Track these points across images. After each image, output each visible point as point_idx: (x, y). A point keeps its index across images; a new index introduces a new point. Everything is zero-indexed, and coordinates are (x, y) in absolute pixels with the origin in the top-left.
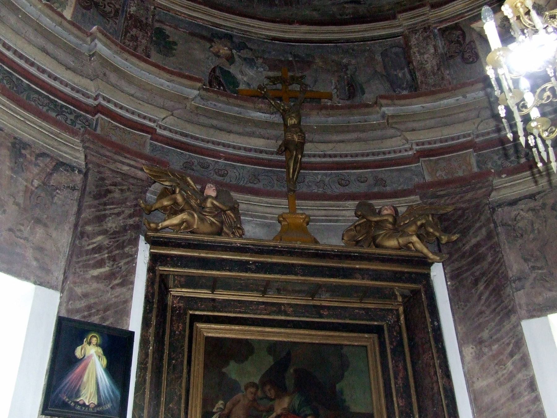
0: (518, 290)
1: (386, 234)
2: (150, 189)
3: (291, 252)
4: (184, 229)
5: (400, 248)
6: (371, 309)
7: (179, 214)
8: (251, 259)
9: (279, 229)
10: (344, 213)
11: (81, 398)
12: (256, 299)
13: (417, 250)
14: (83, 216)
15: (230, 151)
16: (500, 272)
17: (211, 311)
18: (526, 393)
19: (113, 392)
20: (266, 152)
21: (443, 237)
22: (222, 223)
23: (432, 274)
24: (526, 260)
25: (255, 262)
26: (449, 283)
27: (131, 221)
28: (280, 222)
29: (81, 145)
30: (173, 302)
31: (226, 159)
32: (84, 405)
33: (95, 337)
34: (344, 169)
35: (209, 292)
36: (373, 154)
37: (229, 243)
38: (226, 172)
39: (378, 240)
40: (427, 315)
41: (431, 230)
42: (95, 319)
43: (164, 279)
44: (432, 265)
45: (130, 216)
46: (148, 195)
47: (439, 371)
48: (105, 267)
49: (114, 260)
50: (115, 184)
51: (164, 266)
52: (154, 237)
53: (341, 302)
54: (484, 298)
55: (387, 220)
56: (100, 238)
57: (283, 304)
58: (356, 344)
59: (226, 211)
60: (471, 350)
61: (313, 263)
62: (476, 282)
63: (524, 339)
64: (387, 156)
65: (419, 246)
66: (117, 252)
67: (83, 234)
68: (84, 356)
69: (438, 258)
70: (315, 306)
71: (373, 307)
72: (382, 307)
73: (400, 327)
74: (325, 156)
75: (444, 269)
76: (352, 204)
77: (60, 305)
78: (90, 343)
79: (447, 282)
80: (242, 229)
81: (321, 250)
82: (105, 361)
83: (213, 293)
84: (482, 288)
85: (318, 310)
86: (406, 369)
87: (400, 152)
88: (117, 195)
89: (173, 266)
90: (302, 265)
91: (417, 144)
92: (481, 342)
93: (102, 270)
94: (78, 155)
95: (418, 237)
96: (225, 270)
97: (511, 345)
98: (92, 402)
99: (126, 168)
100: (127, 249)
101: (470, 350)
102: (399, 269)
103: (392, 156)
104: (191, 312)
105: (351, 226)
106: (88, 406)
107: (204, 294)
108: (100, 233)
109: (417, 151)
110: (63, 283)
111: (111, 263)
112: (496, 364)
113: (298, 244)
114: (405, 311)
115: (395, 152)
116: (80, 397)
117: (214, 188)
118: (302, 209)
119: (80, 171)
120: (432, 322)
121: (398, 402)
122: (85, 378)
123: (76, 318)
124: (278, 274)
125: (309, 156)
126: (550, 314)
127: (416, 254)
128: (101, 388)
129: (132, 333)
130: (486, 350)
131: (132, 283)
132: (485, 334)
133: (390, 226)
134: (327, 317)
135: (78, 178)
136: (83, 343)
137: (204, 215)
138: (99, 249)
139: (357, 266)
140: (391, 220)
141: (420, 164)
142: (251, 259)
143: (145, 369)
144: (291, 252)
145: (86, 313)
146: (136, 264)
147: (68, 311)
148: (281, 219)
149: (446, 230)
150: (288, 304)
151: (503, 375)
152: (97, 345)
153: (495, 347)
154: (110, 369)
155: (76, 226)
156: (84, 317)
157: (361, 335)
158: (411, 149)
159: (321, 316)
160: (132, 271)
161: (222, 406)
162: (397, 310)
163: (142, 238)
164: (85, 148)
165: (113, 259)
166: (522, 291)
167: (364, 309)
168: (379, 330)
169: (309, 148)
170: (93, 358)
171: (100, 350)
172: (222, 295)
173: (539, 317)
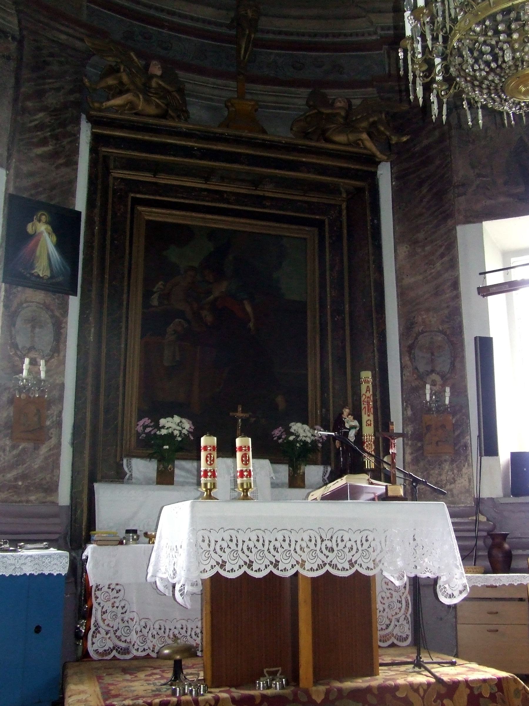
0: (459, 195)
1: (337, 128)
2: (89, 62)
3: (238, 141)
4: (129, 110)
5: (349, 144)
6: (314, 202)
7: (124, 95)
8: (196, 145)
9: (226, 113)
10: (296, 100)
11: (36, 271)
12: (199, 186)
13: (365, 148)
14: (23, 90)
15: (176, 19)
16: (446, 176)
17: (153, 195)
18: (448, 291)
19: (64, 267)
20: (216, 24)
21: (393, 137)
22: (167, 105)
23: (379, 172)
24: (473, 167)
25: (199, 149)
26: (393, 183)
27: (72, 98)
28: (227, 106)
29: (14, 7)
30: (114, 184)
31: (170, 29)
32: (38, 276)
33: (43, 214)
34: (300, 49)
35: (151, 176)
36: (334, 35)
37: (175, 127)
38: (170, 45)
39: (328, 134)
40: (368, 213)
41: (382, 129)
42: (42, 198)
43: (106, 158)
44: (379, 164)
45: (71, 92)
46: (88, 68)
47: (372, 266)
48: (48, 146)
49: (57, 139)
50: (52, 55)
51: (108, 146)
52: (96, 117)
53: (284, 193)
54: (426, 200)
55: (339, 114)
56: (41, 115)
57: (226, 192)
58: (296, 236)
59: (173, 91)
60: (405, 249)
61: (258, 153)
62: (420, 185)
63: (456, 242)
64: (349, 39)
65: (369, 144)
66: (60, 130)
67: (25, 110)
68: (35, 233)
69: (385, 158)
70: (258, 196)
71: (316, 201)
72: (326, 201)
73: (341, 222)
74: (280, 33)
75: (391, 168)
76: (305, 92)
77: (7, 182)
78: (40, 221)
79: (392, 182)
80: (187, 112)
81: (268, 141)
82: (55, 239)
83: (154, 177)
84: (425, 191)
85: (259, 200)
86: (342, 261)
87: (363, 35)
88: (55, 68)
89: (116, 148)
90: (248, 155)
91: (383, 29)
92: (415, 243)
93: (45, 149)
94: (9, 18)
95: (370, 135)
96: (170, 155)
97: (444, 247)
98: (45, 274)
99: (63, 37)
100: (69, 128)
101: (404, 250)
102: (345, 165)
103: (354, 39)
104: (132, 195)
105: (301, 116)
106: (42, 278)
107: (146, 177)
108: (41, 110)
109: (381, 37)
110: (8, 160)
111: (54, 142)
112: (427, 263)
113: (246, 134)
114: (347, 207)
115: (357, 35)
116: (34, 269)
117: (159, 66)
118: (251, 93)
119: (13, 38)
120: (372, 221)
121: (331, 292)
122: (38, 253)
123: (24, 196)
124: (223, 162)
125: (262, 31)
126: (485, 221)
127: (365, 151)
128: (53, 263)
129: (79, 213)
130: (419, 250)
131: (76, 163)
132: (421, 236)
133: (341, 120)
134: (270, 208)
135: (13, 46)
136: (33, 221)
137: (149, 96)
138: (41, 127)
139: (304, 160)
140: (343, 113)
141: (382, 52)
142: (196, 145)
143: (92, 247)
144: (238, 141)
145: (33, 192)
146: (79, 144)
147: (16, 188)
148: (230, 104)
149: (399, 130)
150: (231, 192)
151: (431, 274)
152: (46, 223)
153: (428, 248)
154: (59, 246)
155: (15, 100)
156: (31, 195)
157: (301, 227)
158: (375, 33)
159: (264, 207)
160: (76, 151)
161: (162, 287)
162: (340, 206)
163: (83, 117)
164: (19, 12)
165: (56, 137)
166: (463, 197)
167: (306, 202)
168: (320, 224)
169: (264, 23)
170: (44, 234)
171: (49, 228)
172: (164, 180)
173: (474, 222)
